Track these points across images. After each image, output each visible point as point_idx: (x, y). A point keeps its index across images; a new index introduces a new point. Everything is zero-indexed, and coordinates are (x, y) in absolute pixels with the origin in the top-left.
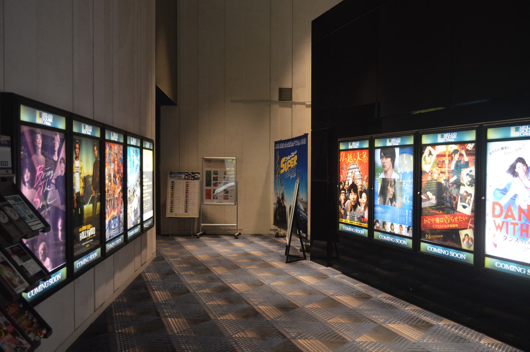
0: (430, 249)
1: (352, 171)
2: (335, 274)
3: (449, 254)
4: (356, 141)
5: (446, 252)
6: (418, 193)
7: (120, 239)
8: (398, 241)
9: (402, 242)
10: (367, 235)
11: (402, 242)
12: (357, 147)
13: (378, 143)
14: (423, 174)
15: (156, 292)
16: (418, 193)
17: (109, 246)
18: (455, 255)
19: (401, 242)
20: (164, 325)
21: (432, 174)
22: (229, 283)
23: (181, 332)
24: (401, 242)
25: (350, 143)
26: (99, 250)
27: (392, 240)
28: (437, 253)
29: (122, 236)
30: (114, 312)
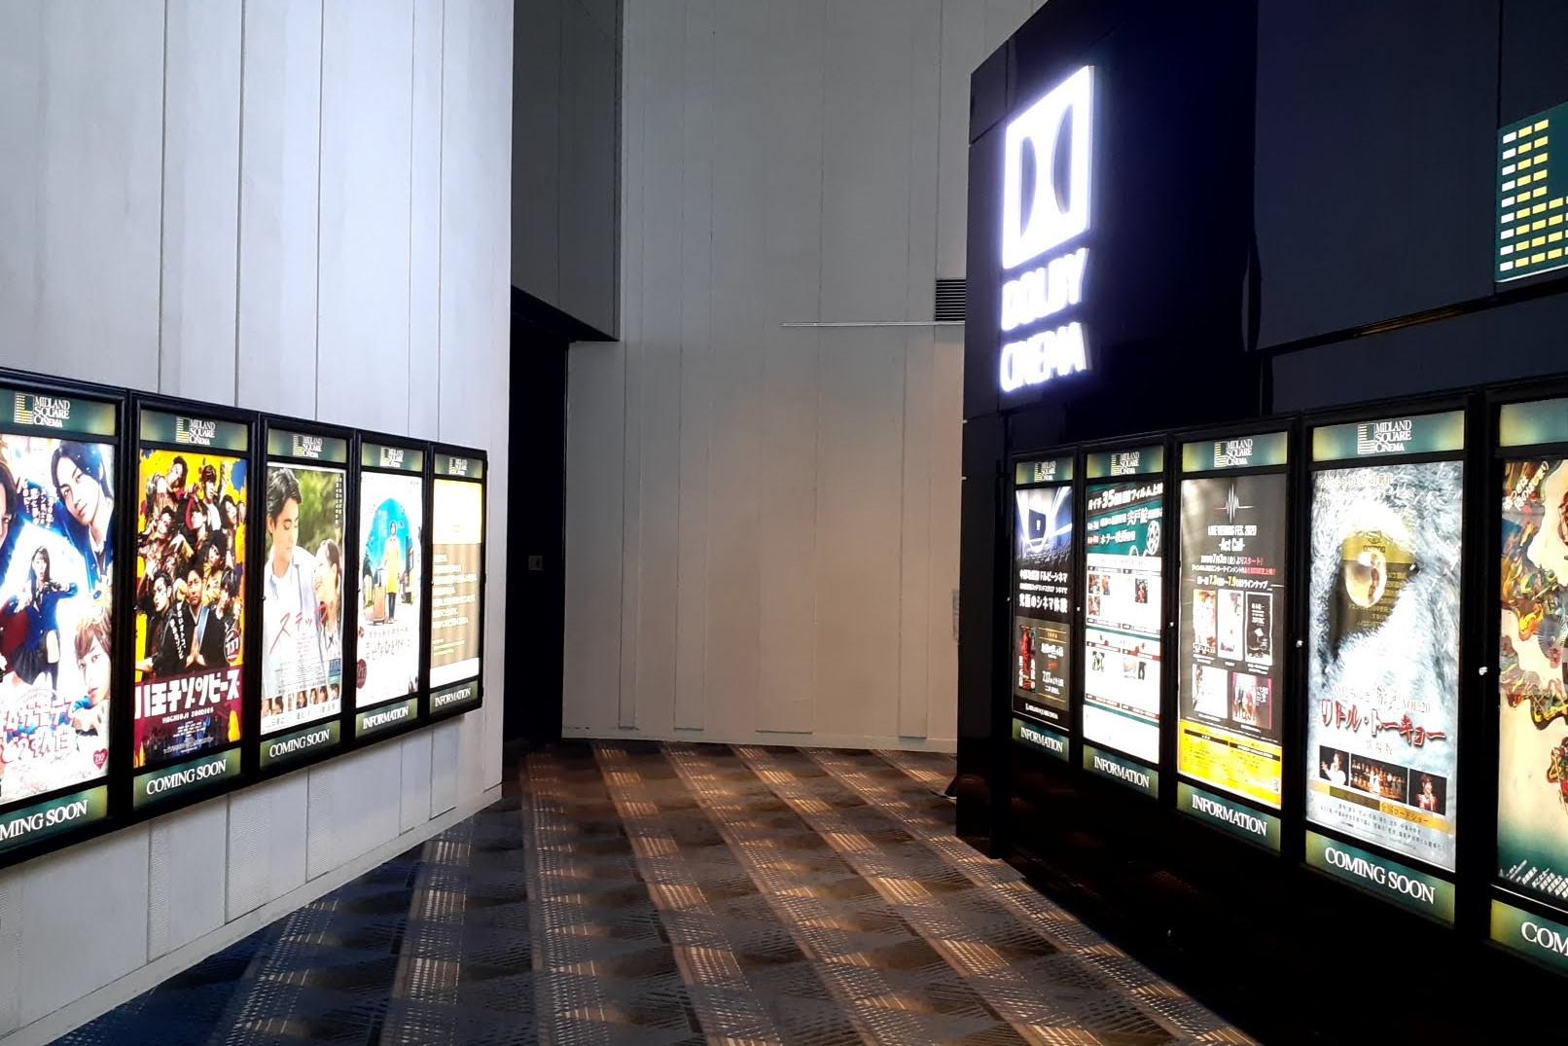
4: (1130, 448)
5: (1379, 873)
7: (405, 711)
8: (1397, 885)
9: (1415, 889)
10: (1277, 843)
11: (1415, 889)
12: (1399, 448)
13: (1190, 462)
16: (1483, 671)
17: (438, 701)
20: (409, 904)
21: (1416, 570)
22: (1024, 1021)
23: (428, 993)
25: (1362, 429)
28: (1351, 873)
29: (414, 702)
30: (242, 1018)
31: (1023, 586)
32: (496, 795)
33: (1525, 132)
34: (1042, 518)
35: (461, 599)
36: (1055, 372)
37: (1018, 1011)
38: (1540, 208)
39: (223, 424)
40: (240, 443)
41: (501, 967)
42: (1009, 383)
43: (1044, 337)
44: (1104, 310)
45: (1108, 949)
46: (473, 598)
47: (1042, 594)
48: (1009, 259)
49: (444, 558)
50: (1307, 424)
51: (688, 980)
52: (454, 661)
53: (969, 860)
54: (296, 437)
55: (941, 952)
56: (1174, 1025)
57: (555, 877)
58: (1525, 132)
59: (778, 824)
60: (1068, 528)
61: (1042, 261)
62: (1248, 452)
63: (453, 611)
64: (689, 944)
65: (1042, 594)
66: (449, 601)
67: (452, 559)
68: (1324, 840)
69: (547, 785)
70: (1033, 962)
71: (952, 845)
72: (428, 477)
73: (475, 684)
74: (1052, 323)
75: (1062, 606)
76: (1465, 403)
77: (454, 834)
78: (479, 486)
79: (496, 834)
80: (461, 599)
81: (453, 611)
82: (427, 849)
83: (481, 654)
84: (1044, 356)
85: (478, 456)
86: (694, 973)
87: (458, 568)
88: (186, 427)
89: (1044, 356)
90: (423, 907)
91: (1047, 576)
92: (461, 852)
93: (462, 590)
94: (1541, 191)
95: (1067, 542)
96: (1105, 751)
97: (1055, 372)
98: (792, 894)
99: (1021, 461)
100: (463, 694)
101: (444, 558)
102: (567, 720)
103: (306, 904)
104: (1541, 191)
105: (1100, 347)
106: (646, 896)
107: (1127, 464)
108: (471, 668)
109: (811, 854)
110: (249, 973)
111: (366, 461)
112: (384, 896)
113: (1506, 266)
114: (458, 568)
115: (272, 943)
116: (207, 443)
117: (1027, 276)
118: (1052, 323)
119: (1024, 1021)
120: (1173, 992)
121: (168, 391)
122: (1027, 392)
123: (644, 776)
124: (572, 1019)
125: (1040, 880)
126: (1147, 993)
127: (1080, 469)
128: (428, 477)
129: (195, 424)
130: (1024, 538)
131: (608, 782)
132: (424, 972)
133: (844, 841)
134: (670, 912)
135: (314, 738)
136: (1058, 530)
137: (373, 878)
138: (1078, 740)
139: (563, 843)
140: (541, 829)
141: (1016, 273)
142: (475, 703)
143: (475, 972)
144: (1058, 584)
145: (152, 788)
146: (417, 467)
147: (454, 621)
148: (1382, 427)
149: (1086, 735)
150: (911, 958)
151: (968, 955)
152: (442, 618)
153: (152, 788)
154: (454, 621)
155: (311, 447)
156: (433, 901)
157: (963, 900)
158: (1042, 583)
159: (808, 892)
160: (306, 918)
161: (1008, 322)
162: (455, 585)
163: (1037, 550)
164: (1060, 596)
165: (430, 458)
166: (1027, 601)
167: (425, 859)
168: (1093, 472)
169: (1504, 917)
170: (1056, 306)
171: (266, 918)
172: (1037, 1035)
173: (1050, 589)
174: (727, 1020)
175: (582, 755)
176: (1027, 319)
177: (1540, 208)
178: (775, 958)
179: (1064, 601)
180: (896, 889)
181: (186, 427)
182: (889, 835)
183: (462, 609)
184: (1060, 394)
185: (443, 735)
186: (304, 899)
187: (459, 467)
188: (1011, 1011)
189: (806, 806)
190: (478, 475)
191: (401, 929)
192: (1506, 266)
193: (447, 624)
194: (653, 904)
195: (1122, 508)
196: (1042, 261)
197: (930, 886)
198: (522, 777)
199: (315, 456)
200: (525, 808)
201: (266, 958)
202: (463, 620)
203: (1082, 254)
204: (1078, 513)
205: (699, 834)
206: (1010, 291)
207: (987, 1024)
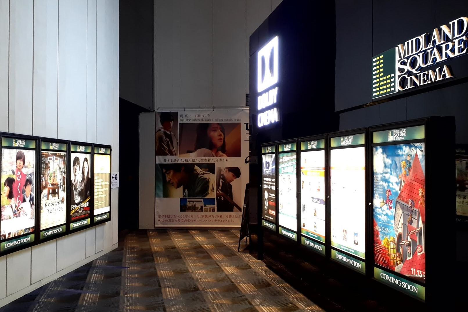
0: (382, 276)
1: (267, 160)
2: (307, 305)
3: (402, 284)
4: (288, 143)
5: (399, 282)
6: (370, 204)
7: (106, 216)
8: (405, 286)
14: (305, 142)
15: (167, 289)
16: (370, 204)
17: (97, 219)
18: (407, 287)
19: (409, 287)
22: (258, 305)
23: (88, 303)
24: (409, 287)
25: (389, 132)
26: (89, 220)
27: (397, 282)
31: (264, 182)
32: (116, 246)
33: (378, 58)
34: (269, 163)
35: (104, 189)
36: (271, 122)
37: (256, 302)
38: (381, 79)
39: (28, 141)
40: (33, 146)
41: (111, 296)
42: (260, 125)
43: (268, 112)
44: (282, 105)
45: (286, 285)
46: (108, 189)
47: (269, 185)
48: (260, 89)
49: (98, 177)
50: (372, 131)
51: (164, 297)
52: (102, 207)
53: (252, 261)
54: (50, 144)
55: (239, 287)
56: (299, 304)
57: (131, 271)
58: (378, 58)
59: (198, 252)
60: (274, 166)
61: (267, 91)
62: (351, 140)
63: (101, 193)
64: (166, 287)
65: (269, 185)
66: (100, 190)
67: (100, 178)
68: (336, 252)
69: (133, 243)
70: (264, 289)
71: (248, 257)
72: (92, 154)
73: (108, 214)
74: (270, 108)
75: (273, 188)
76: (365, 132)
77: (102, 258)
78: (109, 156)
79: (114, 259)
80: (104, 189)
81: (101, 193)
82: (94, 262)
83: (110, 205)
84: (268, 118)
85: (108, 147)
86: (166, 295)
87: (102, 180)
88: (16, 142)
89: (268, 118)
90: (90, 279)
91: (270, 180)
92: (104, 263)
93: (104, 187)
94: (381, 74)
95: (274, 170)
96: (284, 228)
97: (271, 122)
98: (198, 271)
99: (280, 144)
100: (105, 217)
101: (98, 177)
102: (140, 224)
103: (56, 279)
104: (381, 74)
105: (282, 114)
106: (157, 274)
107: (288, 148)
108: (107, 209)
109: (206, 261)
110: (37, 299)
111: (72, 150)
112: (79, 277)
113: (374, 94)
114: (102, 180)
115: (44, 291)
116: (23, 146)
117: (264, 95)
118: (270, 108)
119: (258, 305)
120: (302, 296)
121: (11, 131)
122: (264, 127)
123: (207, 238)
124: (129, 309)
125: (270, 266)
126: (295, 298)
127: (277, 149)
128: (92, 154)
129: (19, 141)
130: (265, 169)
131: (151, 242)
132: (89, 297)
133: (217, 257)
134: (162, 278)
135: (57, 231)
136: (272, 167)
137: (77, 271)
138: (278, 226)
139: (134, 260)
140: (128, 256)
141: (261, 94)
142: (109, 219)
143: (103, 297)
144: (272, 182)
145: (7, 246)
146: (89, 151)
147: (102, 196)
148: (346, 138)
149: (280, 224)
150: (230, 289)
151: (245, 287)
152: (98, 195)
153: (7, 246)
154: (102, 196)
155: (55, 146)
156: (94, 277)
157: (246, 271)
158: (269, 181)
159: (204, 271)
160: (56, 283)
161: (259, 108)
162: (102, 185)
163: (267, 172)
164: (273, 185)
165: (93, 148)
166: (265, 186)
167: (93, 265)
168: (280, 150)
169: (377, 270)
170: (270, 103)
171: (43, 283)
172: (262, 310)
173: (271, 183)
174: (174, 308)
175: (144, 234)
176: (264, 107)
177: (381, 79)
178: (192, 291)
179: (274, 187)
180: (229, 270)
181: (16, 142)
182: (229, 254)
183: (104, 192)
184: (273, 127)
185: (99, 229)
186: (56, 277)
187: (103, 151)
188: (255, 302)
189: (207, 247)
190: (109, 153)
191: (83, 286)
192: (374, 94)
193: (99, 196)
194: (158, 276)
195: (287, 161)
196: (267, 91)
197: (238, 267)
198: (125, 241)
199: (57, 149)
200: (125, 249)
201: (42, 295)
202: (104, 196)
203: (277, 88)
204: (277, 162)
205: (174, 255)
206: (260, 98)
207: (249, 306)
